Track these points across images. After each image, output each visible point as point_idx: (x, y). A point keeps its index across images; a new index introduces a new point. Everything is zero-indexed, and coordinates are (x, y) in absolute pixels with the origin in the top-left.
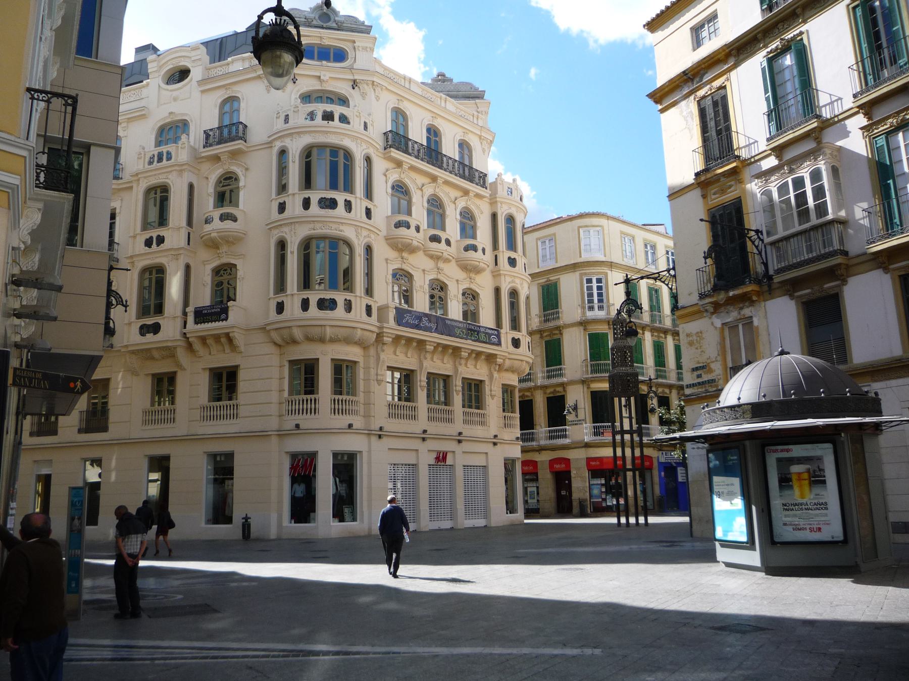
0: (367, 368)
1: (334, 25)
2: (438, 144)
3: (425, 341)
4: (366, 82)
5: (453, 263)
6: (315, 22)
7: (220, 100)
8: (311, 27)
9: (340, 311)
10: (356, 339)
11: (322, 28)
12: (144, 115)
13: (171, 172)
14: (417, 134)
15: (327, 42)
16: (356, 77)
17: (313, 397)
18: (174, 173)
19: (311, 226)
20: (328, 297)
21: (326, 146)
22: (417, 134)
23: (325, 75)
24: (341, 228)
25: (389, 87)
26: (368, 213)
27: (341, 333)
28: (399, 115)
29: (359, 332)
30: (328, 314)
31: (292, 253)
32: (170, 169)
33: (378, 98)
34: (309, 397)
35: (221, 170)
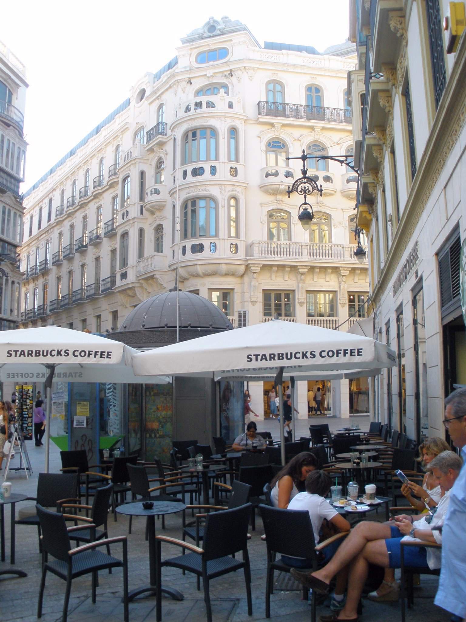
0: (243, 293)
1: (218, 32)
2: (320, 99)
3: (297, 266)
4: (239, 69)
5: (338, 195)
6: (205, 35)
7: (267, 80)
8: (203, 39)
9: (206, 253)
10: (224, 272)
11: (213, 36)
12: (127, 128)
13: (130, 166)
14: (296, 96)
15: (213, 47)
16: (231, 68)
17: (334, 319)
18: (132, 166)
19: (187, 191)
20: (197, 243)
21: (206, 128)
22: (296, 96)
23: (209, 73)
24: (208, 188)
25: (260, 67)
26: (234, 172)
27: (210, 269)
28: (276, 86)
29: (199, 268)
30: (199, 256)
31: (223, 207)
32: (128, 165)
33: (251, 78)
34: (331, 318)
35: (273, 134)
